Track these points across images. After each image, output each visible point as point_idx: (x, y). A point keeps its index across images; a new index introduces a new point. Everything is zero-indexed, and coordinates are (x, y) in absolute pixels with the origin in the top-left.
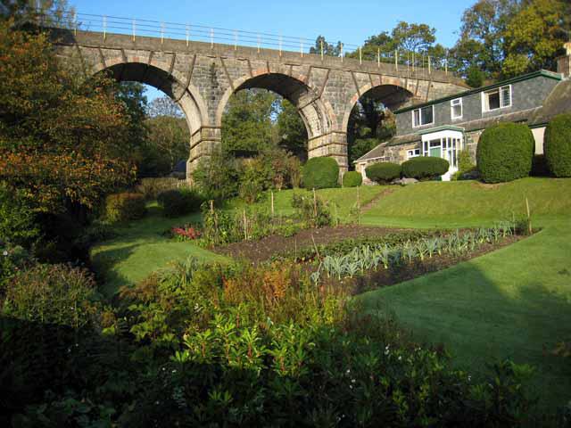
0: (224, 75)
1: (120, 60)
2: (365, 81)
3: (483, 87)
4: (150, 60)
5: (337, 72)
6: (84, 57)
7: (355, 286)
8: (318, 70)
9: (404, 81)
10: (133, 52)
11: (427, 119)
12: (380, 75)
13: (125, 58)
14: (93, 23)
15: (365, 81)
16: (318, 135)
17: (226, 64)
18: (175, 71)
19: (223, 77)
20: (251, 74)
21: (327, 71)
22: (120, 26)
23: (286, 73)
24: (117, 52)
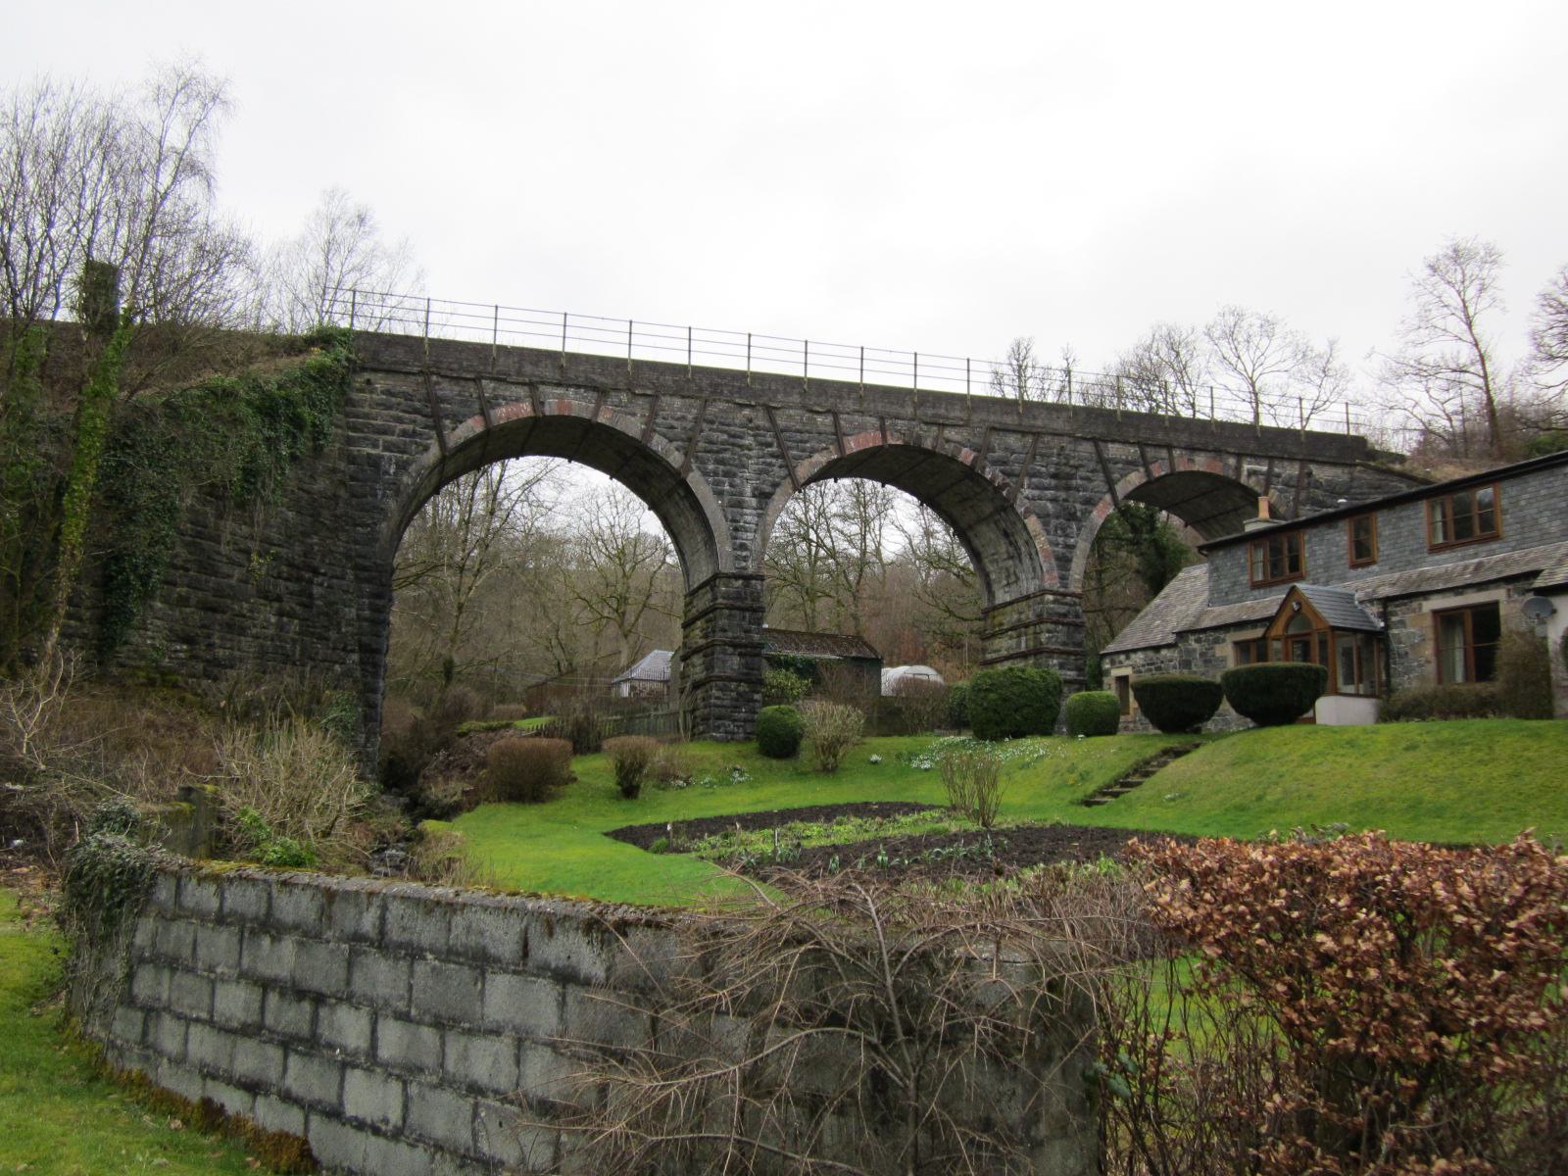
0: (774, 449)
1: (525, 409)
2: (1131, 464)
3: (471, 1143)
4: (884, 437)
5: (1056, 442)
6: (1109, 460)
7: (207, 1141)
8: (1012, 440)
9: (1232, 461)
10: (560, 391)
11: (1113, 663)
12: (1169, 447)
13: (537, 404)
14: (455, 320)
15: (1131, 464)
16: (1008, 598)
17: (781, 422)
18: (656, 437)
19: (772, 455)
20: (841, 447)
21: (1029, 439)
22: (659, 342)
23: (928, 444)
24: (522, 391)
